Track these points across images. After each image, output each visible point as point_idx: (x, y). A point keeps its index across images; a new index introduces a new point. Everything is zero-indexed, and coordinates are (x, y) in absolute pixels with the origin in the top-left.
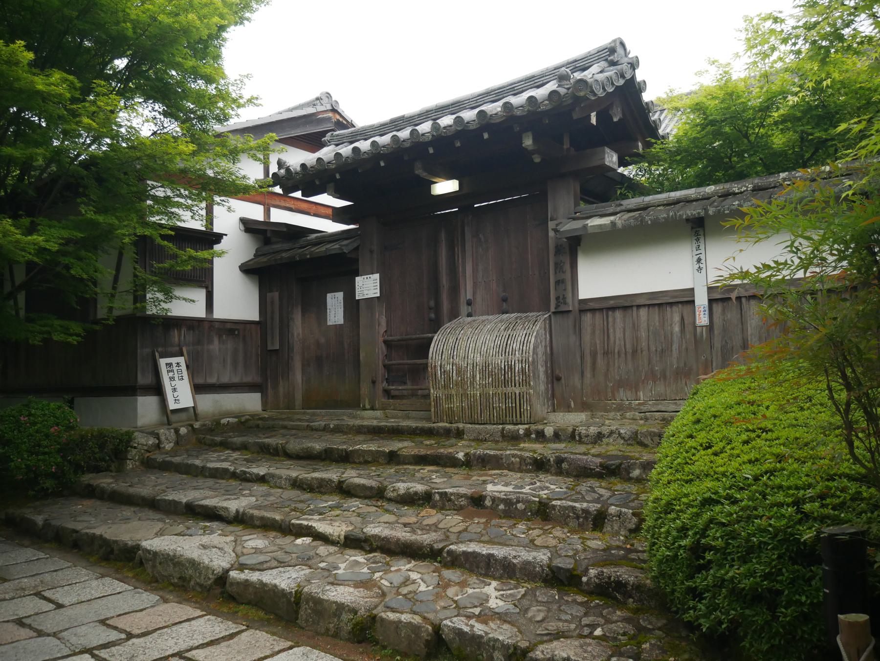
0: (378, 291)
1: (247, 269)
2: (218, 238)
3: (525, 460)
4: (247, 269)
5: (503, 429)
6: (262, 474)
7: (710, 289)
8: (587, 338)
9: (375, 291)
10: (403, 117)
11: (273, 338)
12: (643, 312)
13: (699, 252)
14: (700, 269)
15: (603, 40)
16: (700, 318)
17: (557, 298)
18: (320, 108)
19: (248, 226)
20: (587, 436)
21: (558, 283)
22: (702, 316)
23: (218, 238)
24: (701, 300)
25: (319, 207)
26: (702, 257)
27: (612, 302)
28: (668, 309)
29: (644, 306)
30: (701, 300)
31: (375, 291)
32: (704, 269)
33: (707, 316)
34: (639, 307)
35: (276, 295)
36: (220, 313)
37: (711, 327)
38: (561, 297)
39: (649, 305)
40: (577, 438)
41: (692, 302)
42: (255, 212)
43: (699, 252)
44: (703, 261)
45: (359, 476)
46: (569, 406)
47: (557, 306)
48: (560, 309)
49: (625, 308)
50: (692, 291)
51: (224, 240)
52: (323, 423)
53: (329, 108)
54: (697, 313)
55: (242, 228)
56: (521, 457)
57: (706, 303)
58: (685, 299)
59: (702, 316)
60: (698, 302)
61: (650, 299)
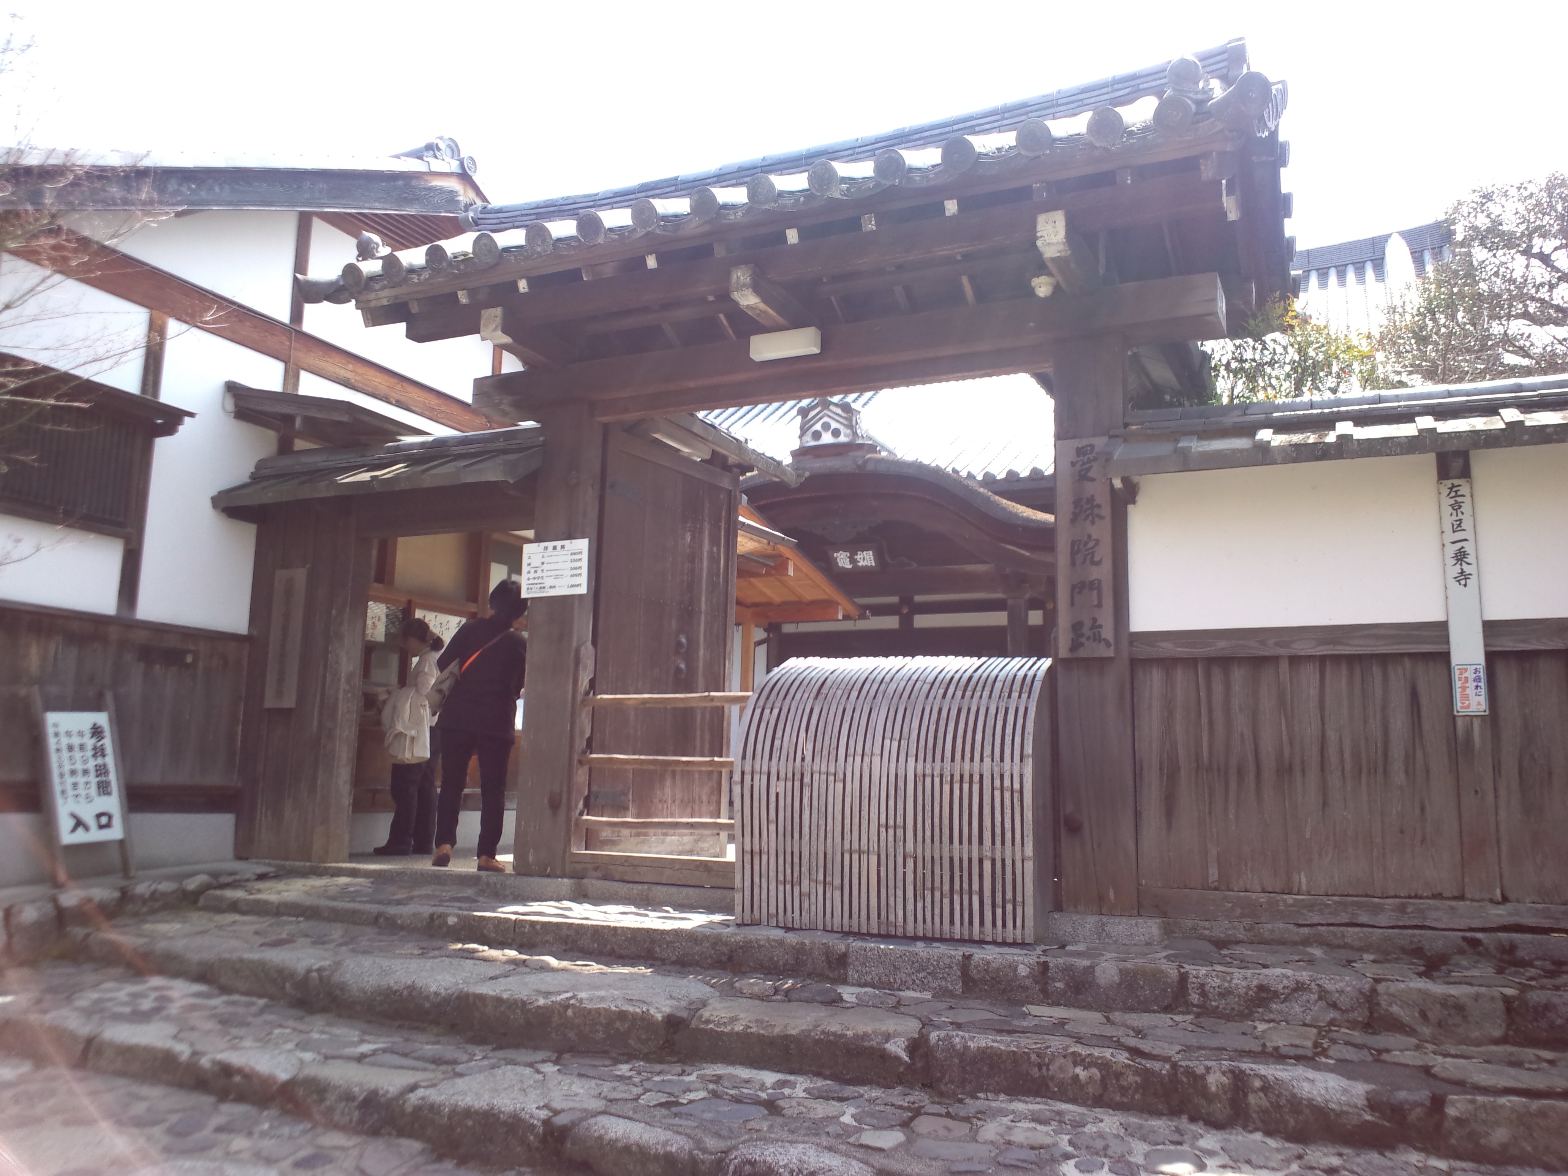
0: (583, 580)
1: (231, 505)
2: (172, 419)
3: (1118, 1075)
4: (231, 505)
5: (968, 958)
6: (283, 1076)
7: (1491, 628)
8: (1151, 726)
9: (576, 581)
10: (676, 179)
11: (281, 680)
12: (1309, 675)
13: (1459, 536)
14: (1463, 578)
15: (1214, 40)
16: (1466, 697)
17: (1077, 627)
18: (437, 166)
19: (244, 403)
20: (1225, 994)
21: (1079, 588)
22: (1471, 691)
23: (172, 419)
24: (1468, 652)
25: (410, 388)
26: (1469, 547)
27: (1222, 644)
28: (1377, 671)
29: (1310, 658)
30: (1468, 652)
31: (576, 581)
32: (1474, 578)
33: (1483, 691)
34: (1295, 660)
35: (300, 575)
36: (151, 607)
37: (1493, 717)
38: (1088, 624)
39: (1323, 659)
40: (1194, 998)
41: (1445, 657)
42: (264, 374)
43: (1459, 536)
44: (1471, 559)
45: (628, 1109)
46: (1101, 899)
47: (1075, 646)
48: (1082, 653)
49: (1258, 662)
50: (1440, 629)
51: (187, 426)
52: (426, 910)
53: (454, 167)
54: (1458, 684)
55: (230, 405)
56: (1104, 1066)
57: (1480, 658)
58: (1420, 650)
59: (1471, 691)
60: (1456, 659)
61: (1324, 642)
